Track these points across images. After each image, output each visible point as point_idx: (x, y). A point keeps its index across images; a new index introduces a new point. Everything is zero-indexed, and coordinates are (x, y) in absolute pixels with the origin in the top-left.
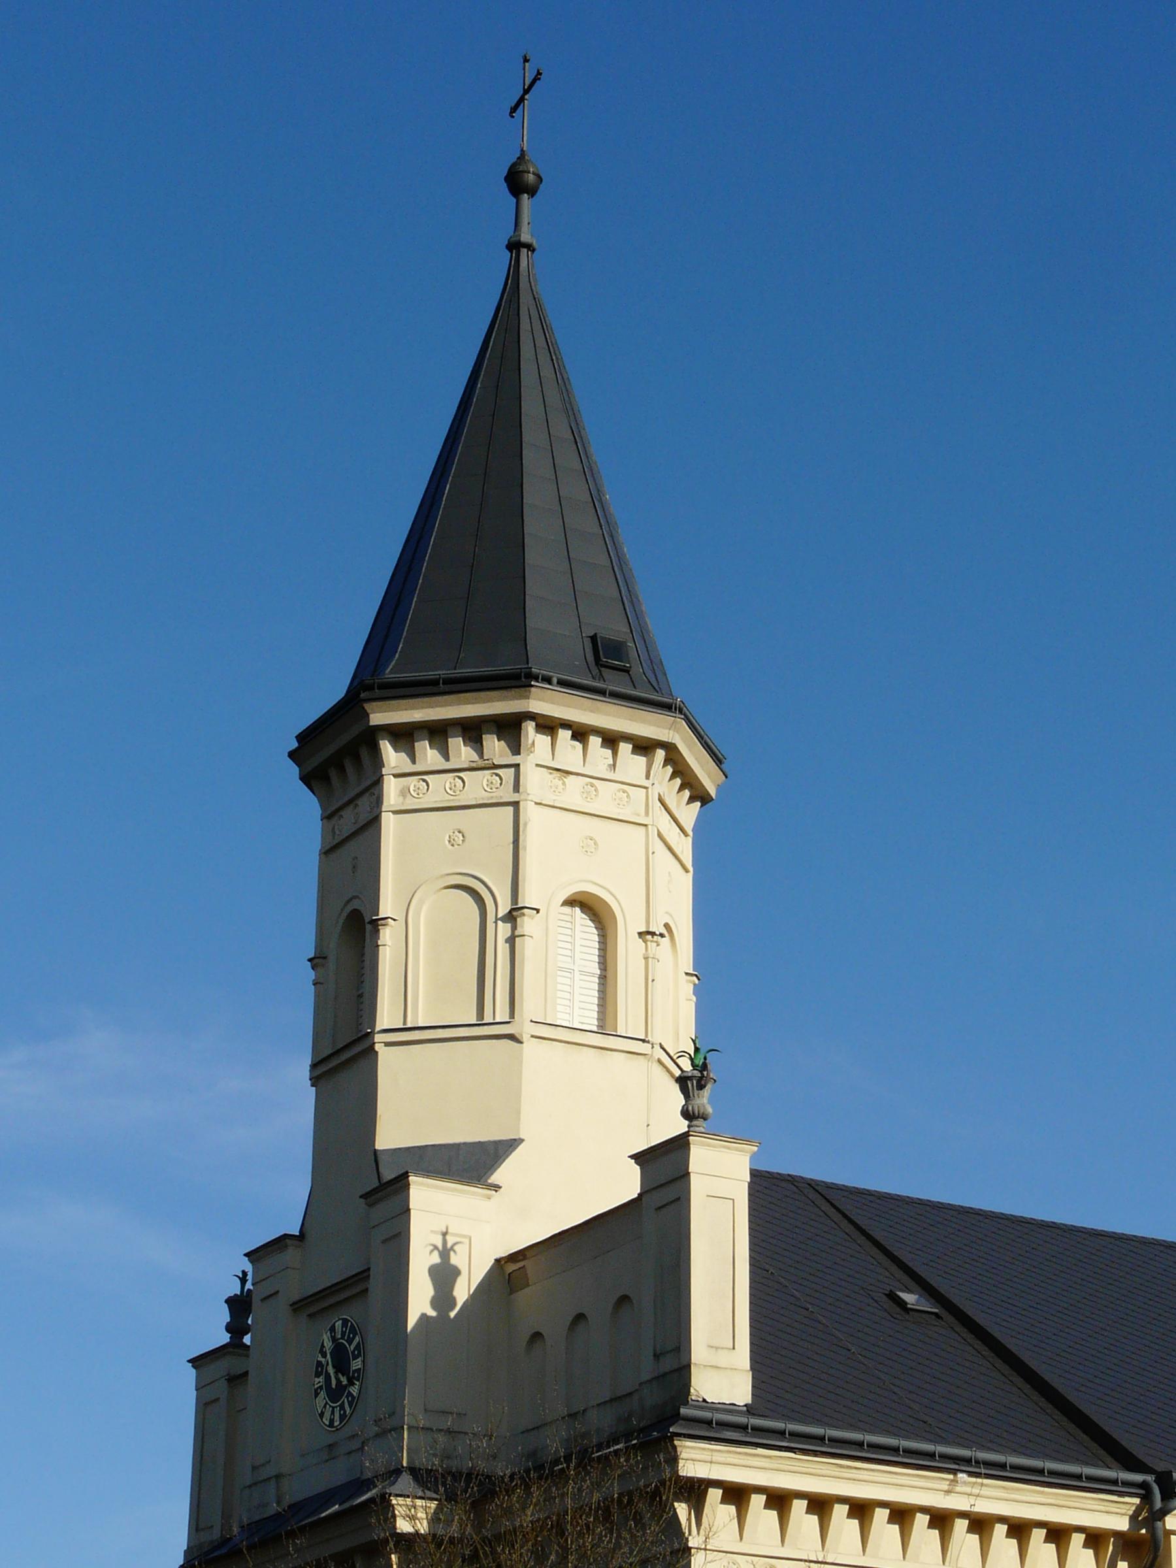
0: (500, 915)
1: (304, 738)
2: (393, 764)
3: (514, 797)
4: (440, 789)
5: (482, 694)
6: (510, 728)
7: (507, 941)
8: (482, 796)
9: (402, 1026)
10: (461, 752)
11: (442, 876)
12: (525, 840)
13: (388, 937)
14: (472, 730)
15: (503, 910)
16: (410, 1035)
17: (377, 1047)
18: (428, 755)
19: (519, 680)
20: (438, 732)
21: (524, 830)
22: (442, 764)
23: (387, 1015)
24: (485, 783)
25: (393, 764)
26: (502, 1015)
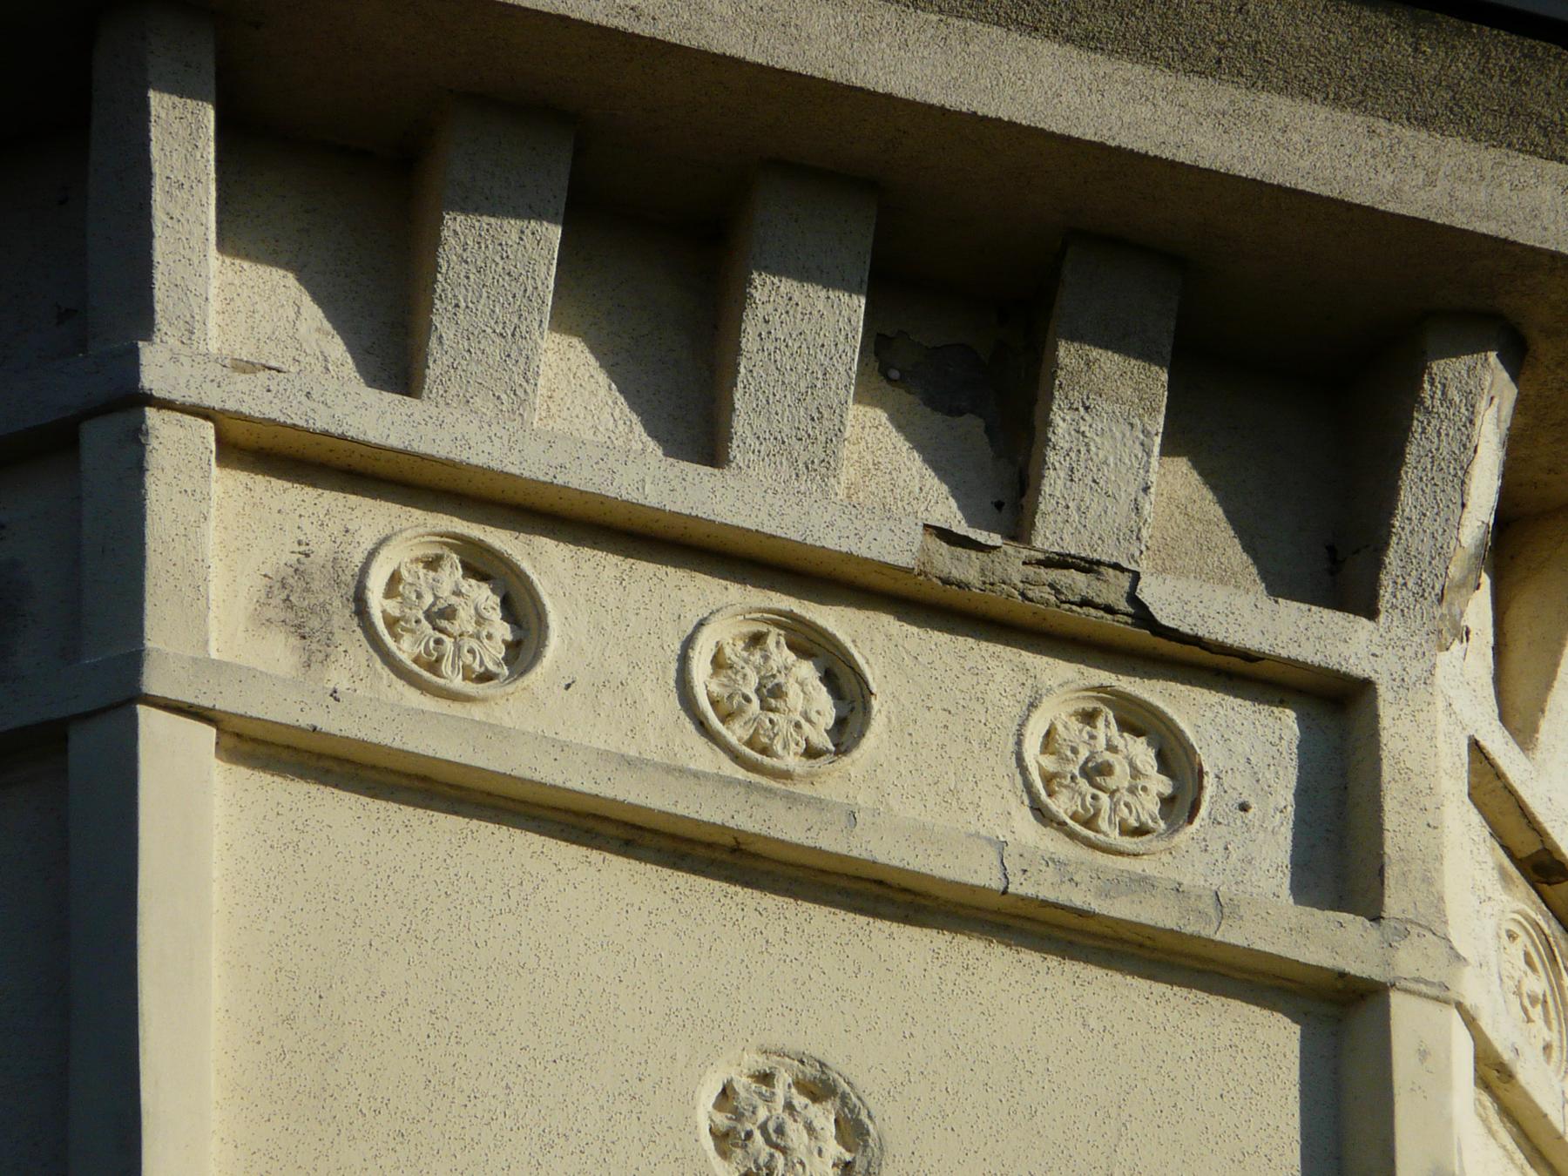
4: (615, 677)
8: (973, 830)
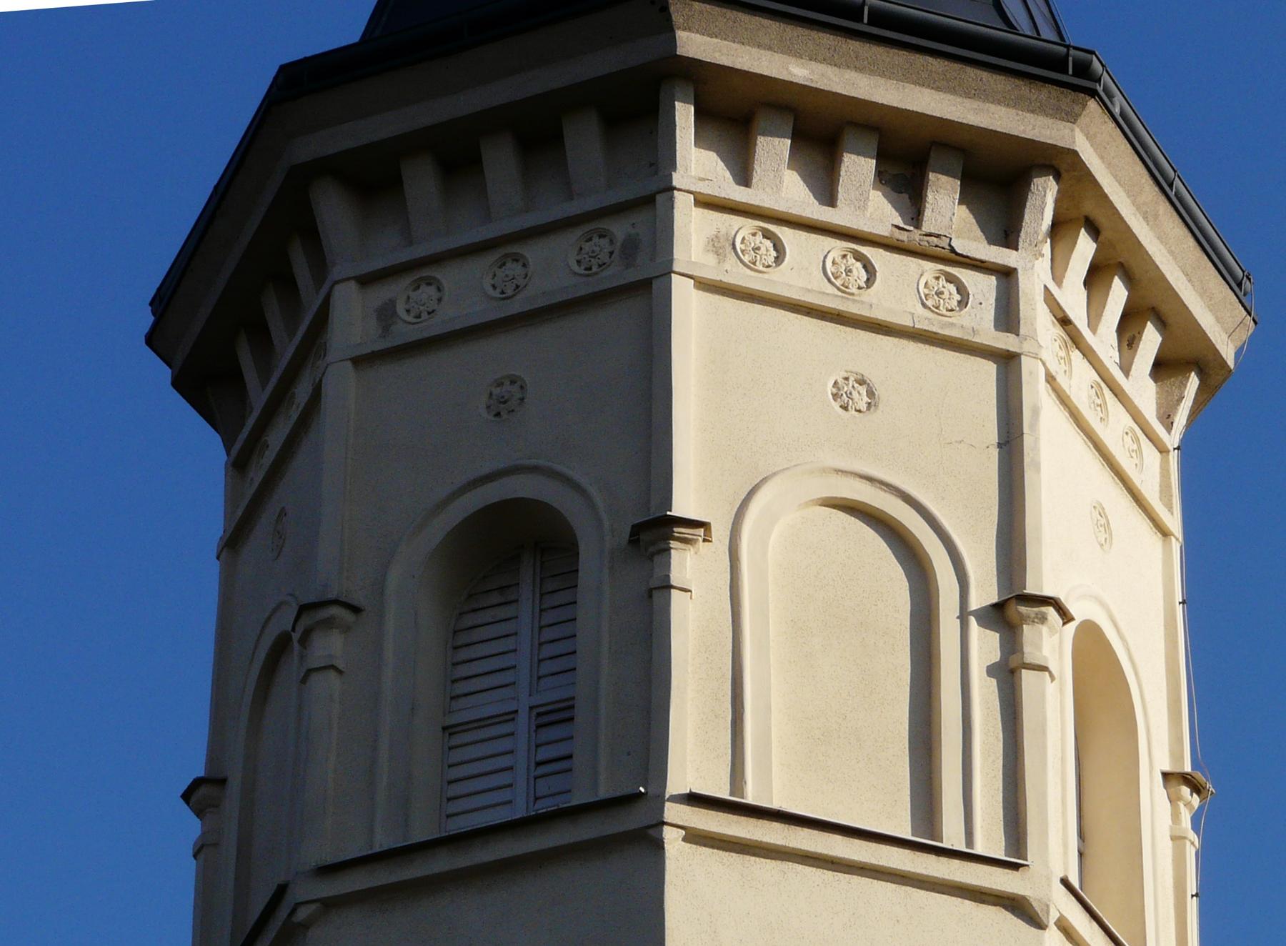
0: (975, 603)
1: (163, 302)
2: (693, 172)
3: (1005, 342)
4: (806, 265)
5: (972, 74)
6: (998, 178)
7: (992, 671)
9: (724, 793)
10: (864, 199)
11: (824, 471)
12: (1036, 448)
13: (690, 566)
14: (908, 157)
15: (984, 592)
16: (746, 823)
17: (672, 838)
18: (780, 179)
19: (1061, 71)
20: (822, 133)
21: (1034, 426)
22: (814, 210)
23: (692, 762)
24: (487, 283)
25: (693, 172)
26: (990, 841)
